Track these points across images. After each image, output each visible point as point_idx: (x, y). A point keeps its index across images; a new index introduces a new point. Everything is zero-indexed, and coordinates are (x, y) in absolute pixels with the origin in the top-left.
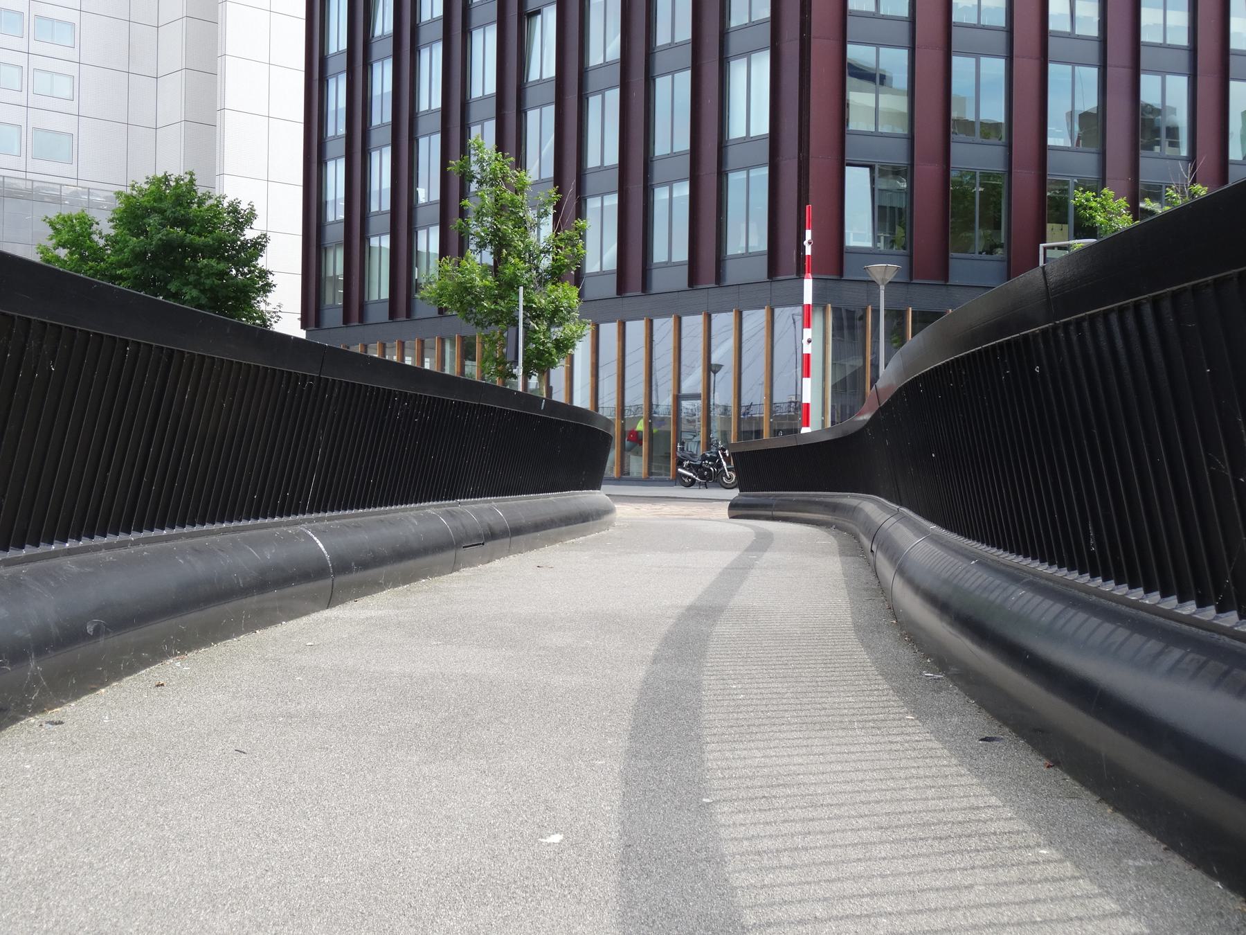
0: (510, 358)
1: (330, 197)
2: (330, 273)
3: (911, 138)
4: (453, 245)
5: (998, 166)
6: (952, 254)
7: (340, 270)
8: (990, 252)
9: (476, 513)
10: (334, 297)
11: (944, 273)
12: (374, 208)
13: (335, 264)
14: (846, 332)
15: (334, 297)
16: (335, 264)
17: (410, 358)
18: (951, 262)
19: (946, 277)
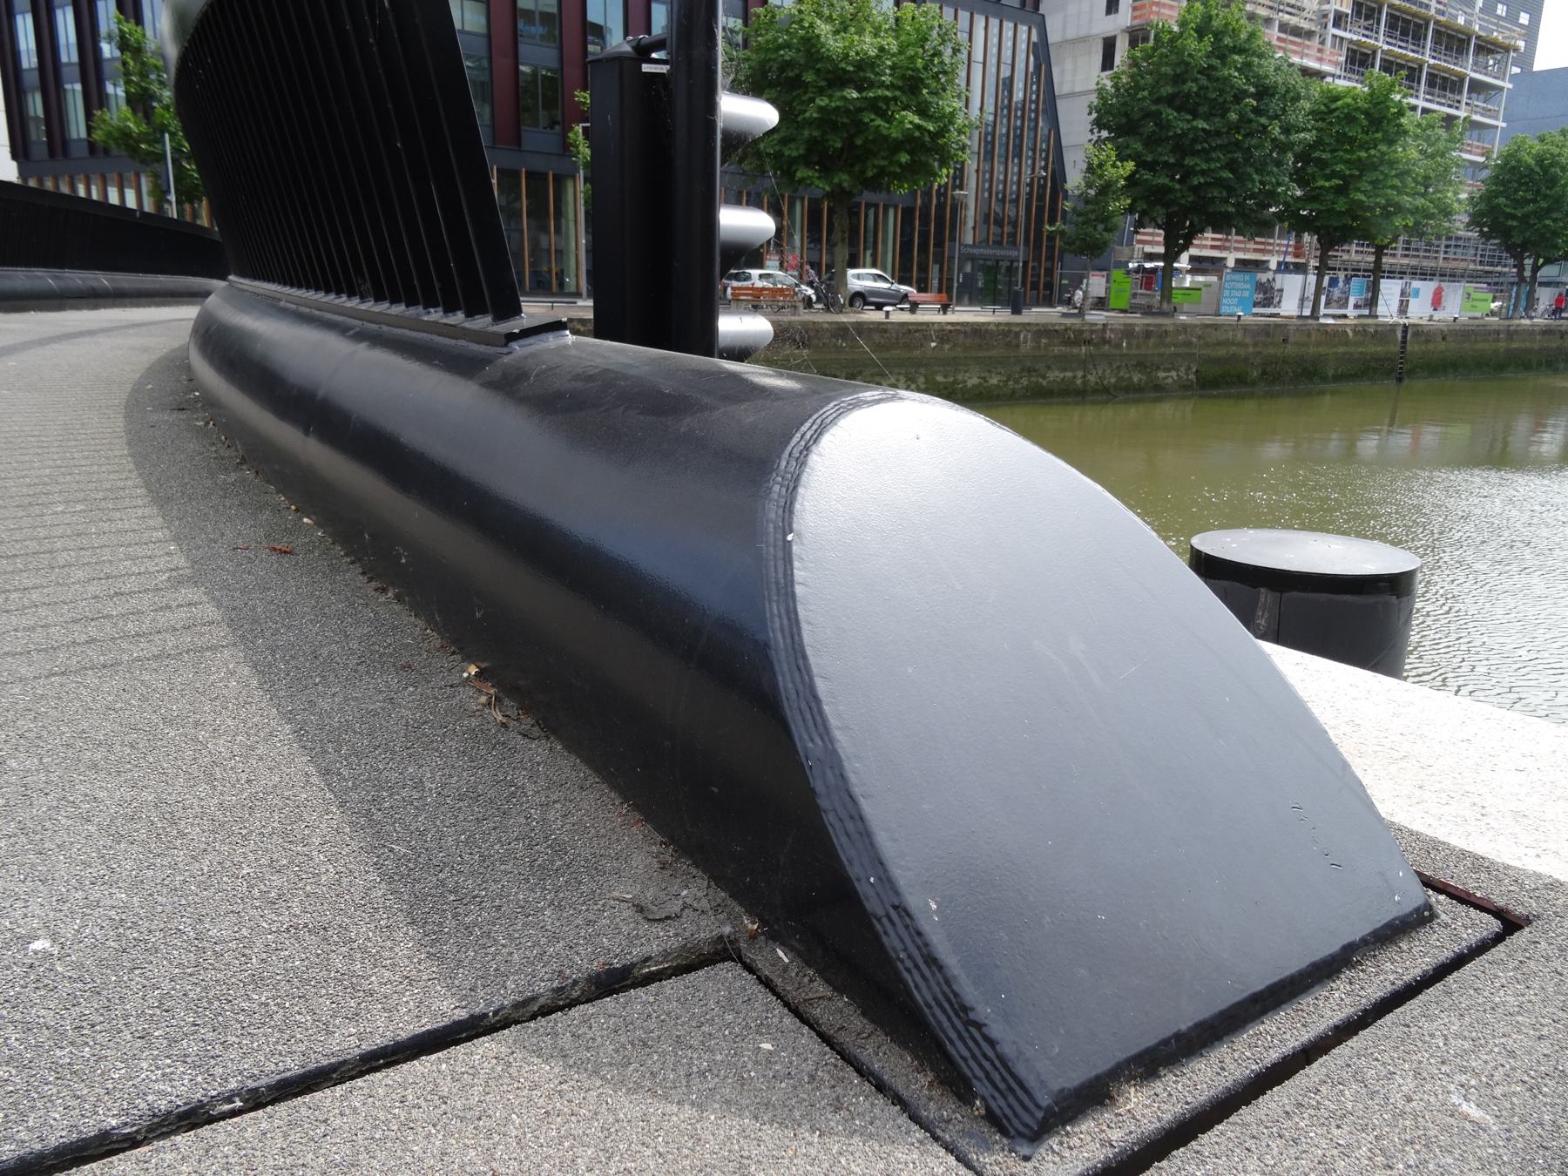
0: (164, 188)
1: (23, 46)
2: (32, 113)
3: (489, 36)
4: (95, 99)
5: (555, 65)
6: (523, 128)
7: (40, 113)
8: (552, 128)
9: (81, 279)
10: (38, 134)
11: (518, 141)
12: (64, 59)
13: (35, 105)
14: (1468, 69)
15: (38, 134)
16: (35, 105)
17: (1527, 16)
18: (523, 133)
19: (519, 145)
